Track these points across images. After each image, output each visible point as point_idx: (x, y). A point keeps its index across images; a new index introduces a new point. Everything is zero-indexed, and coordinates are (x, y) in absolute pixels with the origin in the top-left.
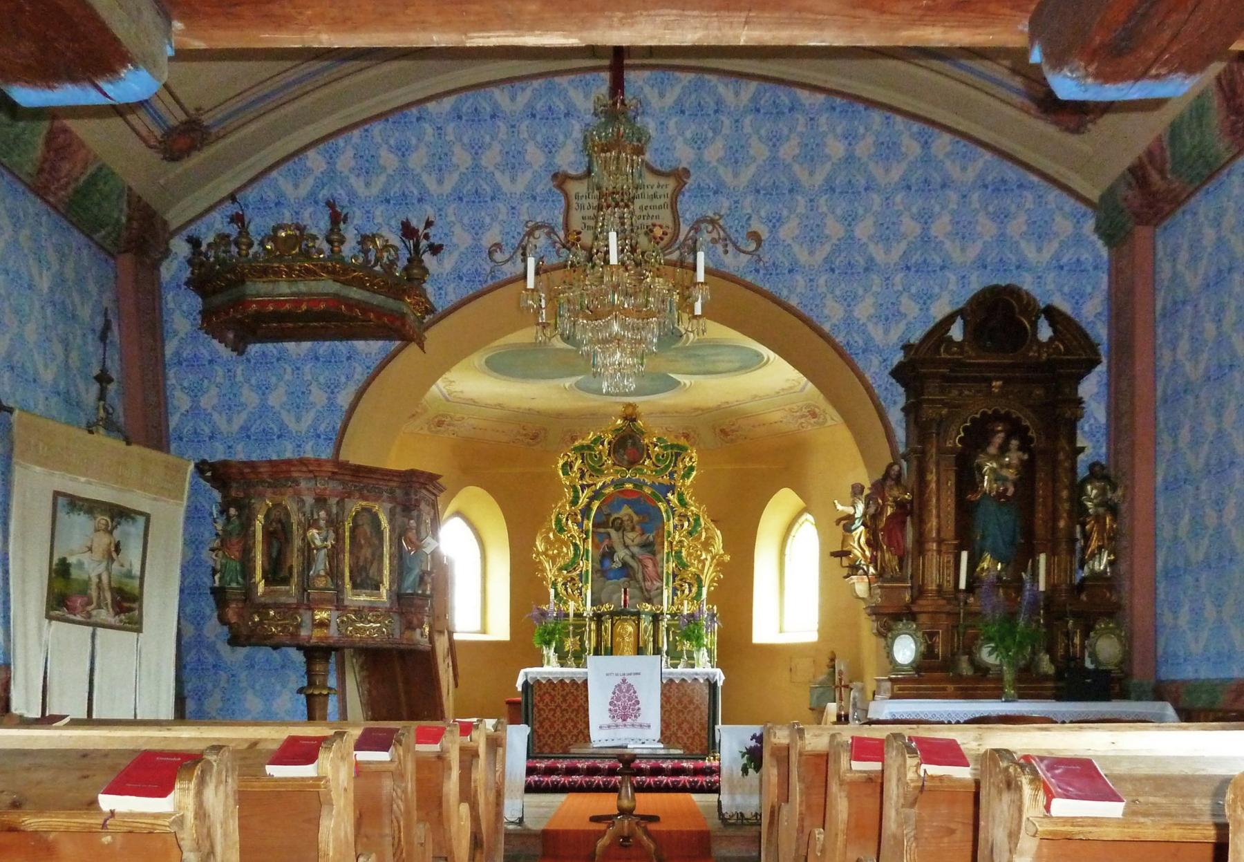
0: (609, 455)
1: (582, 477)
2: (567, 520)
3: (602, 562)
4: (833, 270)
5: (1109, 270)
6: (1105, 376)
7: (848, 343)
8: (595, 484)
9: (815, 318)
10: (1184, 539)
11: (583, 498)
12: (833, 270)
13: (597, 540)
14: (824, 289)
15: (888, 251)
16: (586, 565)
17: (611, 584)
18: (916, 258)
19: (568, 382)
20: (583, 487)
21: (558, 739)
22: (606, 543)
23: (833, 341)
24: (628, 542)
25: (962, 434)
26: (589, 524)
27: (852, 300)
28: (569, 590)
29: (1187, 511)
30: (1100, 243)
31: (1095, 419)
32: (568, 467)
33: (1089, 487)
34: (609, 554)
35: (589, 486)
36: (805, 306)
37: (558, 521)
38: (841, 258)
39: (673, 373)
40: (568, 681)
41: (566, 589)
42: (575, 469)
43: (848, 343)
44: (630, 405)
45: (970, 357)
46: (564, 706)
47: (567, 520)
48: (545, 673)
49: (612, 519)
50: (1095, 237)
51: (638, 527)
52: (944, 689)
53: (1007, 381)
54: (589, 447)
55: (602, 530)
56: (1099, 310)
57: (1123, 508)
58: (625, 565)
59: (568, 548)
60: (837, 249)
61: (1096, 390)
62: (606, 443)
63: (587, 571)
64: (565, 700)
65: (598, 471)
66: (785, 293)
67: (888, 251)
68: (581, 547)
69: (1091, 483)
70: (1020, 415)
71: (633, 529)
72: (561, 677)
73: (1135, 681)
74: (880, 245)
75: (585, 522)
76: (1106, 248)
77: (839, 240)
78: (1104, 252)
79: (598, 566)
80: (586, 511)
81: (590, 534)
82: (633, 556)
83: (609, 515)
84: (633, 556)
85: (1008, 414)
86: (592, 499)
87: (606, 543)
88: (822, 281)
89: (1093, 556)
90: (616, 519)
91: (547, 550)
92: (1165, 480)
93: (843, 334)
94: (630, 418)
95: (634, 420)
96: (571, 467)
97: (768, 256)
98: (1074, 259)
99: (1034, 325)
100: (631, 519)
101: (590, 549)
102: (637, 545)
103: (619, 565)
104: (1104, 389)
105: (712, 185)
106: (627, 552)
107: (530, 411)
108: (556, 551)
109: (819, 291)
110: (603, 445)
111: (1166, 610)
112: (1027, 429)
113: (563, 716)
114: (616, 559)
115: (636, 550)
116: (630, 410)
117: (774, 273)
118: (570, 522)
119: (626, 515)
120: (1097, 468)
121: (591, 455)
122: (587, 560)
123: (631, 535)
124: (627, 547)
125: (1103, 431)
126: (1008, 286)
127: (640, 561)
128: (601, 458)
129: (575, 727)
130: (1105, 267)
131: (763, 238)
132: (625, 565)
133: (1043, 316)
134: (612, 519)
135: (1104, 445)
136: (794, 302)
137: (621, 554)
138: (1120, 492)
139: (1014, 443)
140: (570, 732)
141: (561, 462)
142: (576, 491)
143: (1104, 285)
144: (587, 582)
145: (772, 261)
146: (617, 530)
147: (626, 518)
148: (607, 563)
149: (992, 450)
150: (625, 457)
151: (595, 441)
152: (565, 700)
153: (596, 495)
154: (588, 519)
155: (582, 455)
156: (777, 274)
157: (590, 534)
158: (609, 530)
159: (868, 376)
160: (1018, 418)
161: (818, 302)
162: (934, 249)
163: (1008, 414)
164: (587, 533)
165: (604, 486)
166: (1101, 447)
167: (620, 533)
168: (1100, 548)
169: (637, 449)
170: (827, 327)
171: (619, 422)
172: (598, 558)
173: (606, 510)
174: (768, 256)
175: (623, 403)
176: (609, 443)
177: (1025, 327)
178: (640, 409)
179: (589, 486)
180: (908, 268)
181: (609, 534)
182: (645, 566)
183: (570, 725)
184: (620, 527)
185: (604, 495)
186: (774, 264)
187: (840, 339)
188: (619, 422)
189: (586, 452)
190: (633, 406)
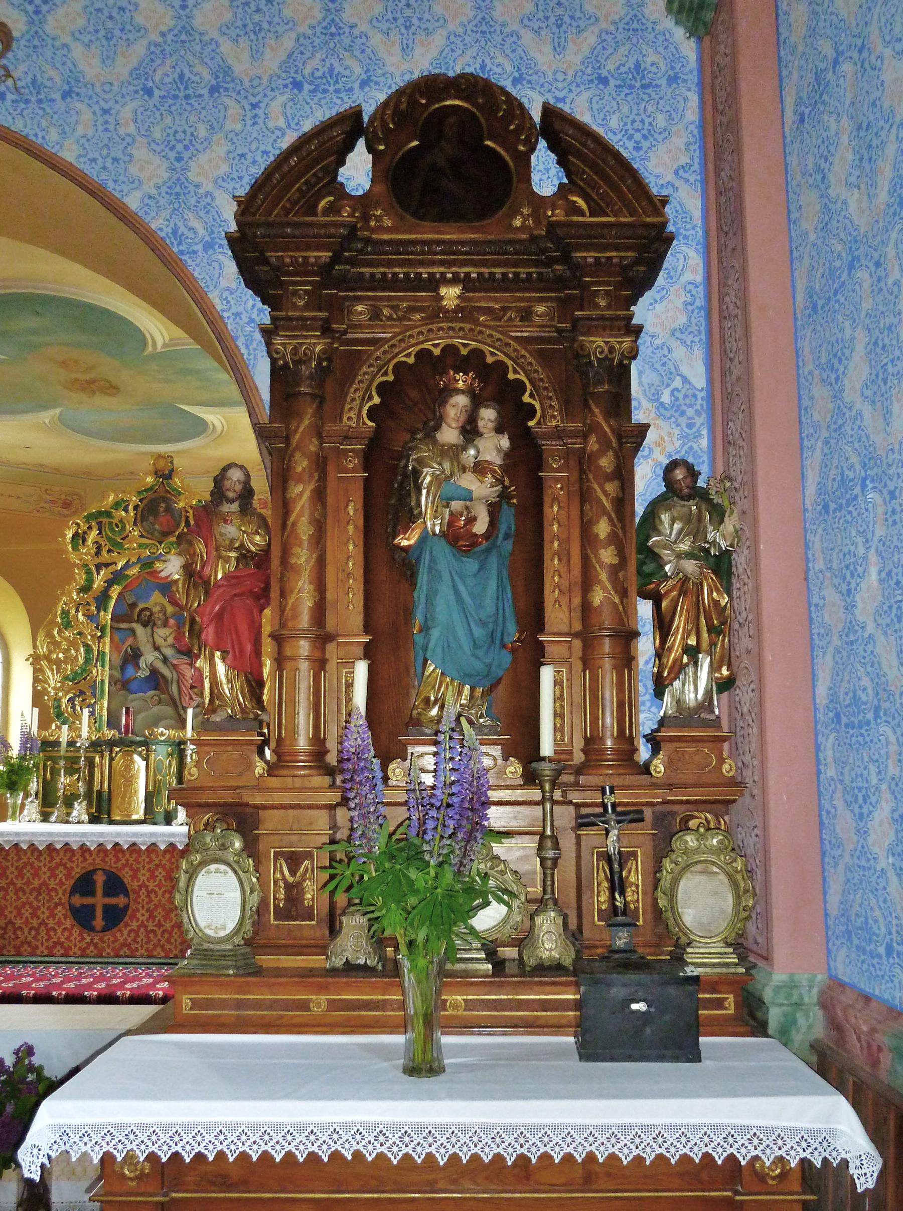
0: (135, 524)
1: (98, 553)
2: (77, 611)
3: (123, 668)
4: (149, 92)
5: (701, 84)
6: (700, 292)
7: (175, 232)
8: (115, 563)
9: (110, 185)
10: (871, 628)
11: (99, 581)
12: (149, 92)
13: (117, 638)
14: (132, 129)
15: (256, 55)
16: (102, 674)
17: (135, 700)
18: (314, 65)
19: (47, 416)
20: (98, 567)
21: (43, 933)
22: (130, 641)
23: (145, 226)
24: (159, 641)
25: (377, 400)
26: (106, 617)
27: (186, 148)
28: (78, 708)
29: (873, 557)
30: (679, 33)
31: (685, 380)
32: (79, 538)
33: (665, 517)
34: (134, 656)
35: (107, 565)
36: (94, 160)
37: (65, 613)
38: (167, 68)
39: (183, 404)
40: (24, 847)
41: (73, 707)
42: (90, 542)
43: (175, 232)
44: (159, 456)
45: (381, 229)
46: (19, 883)
47: (77, 611)
48: (9, 834)
49: (138, 609)
50: (668, 23)
51: (172, 621)
52: (304, 1006)
53: (467, 284)
54: (108, 514)
55: (124, 626)
56: (684, 160)
57: (740, 560)
58: (154, 672)
59: (77, 651)
60: (156, 53)
61: (682, 319)
62: (131, 508)
63: (102, 681)
64: (21, 875)
65: (116, 546)
66: (53, 136)
67: (256, 55)
68: (95, 648)
69: (668, 509)
70: (502, 357)
71: (165, 624)
72: (15, 839)
73: (779, 977)
74: (244, 42)
75: (102, 614)
76: (692, 43)
77: (163, 35)
78: (689, 49)
79: (117, 674)
80: (102, 599)
81: (108, 630)
82: (165, 660)
83: (133, 605)
84: (165, 660)
85: (477, 354)
86: (110, 583)
87: (130, 641)
88: (126, 113)
89: (678, 669)
90: (143, 610)
91: (50, 652)
92: (821, 489)
93: (166, 214)
94: (165, 474)
95: (169, 476)
96: (84, 540)
97: (23, 68)
98: (631, 64)
99: (524, 161)
100: (163, 610)
101: (107, 650)
102: (172, 646)
103: (143, 673)
104: (700, 319)
105: (509, 69)
106: (156, 654)
107: (57, 471)
108: (61, 655)
109: (122, 131)
110: (126, 511)
111: (839, 803)
112: (520, 387)
113: (18, 899)
114: (142, 664)
115: (169, 652)
116: (161, 464)
117: (34, 99)
118: (80, 614)
119: (156, 604)
120: (679, 474)
121: (111, 523)
122: (103, 666)
123: (161, 632)
124: (157, 648)
125: (700, 402)
126: (462, 76)
127: (175, 667)
128: (124, 528)
129: (34, 914)
130: (694, 78)
131: (15, 34)
132: (154, 672)
133: (542, 144)
134: (138, 609)
135: (705, 432)
136: (69, 154)
137: (149, 657)
138: (729, 525)
139: (488, 415)
140: (27, 922)
141: (69, 534)
142: (89, 573)
143: (692, 114)
144: (102, 697)
145: (30, 76)
146: (145, 625)
147: (156, 609)
148: (130, 671)
149: (449, 435)
150: (157, 527)
151: (117, 505)
152: (21, 875)
153: (116, 578)
154: (105, 610)
155: (100, 524)
156: (40, 101)
157: (108, 630)
158: (134, 625)
159: (214, 296)
160: (501, 365)
161: (117, 152)
162: (349, 49)
163: (477, 354)
164: (103, 631)
165: (127, 566)
166: (698, 436)
167: (149, 629)
168: (693, 652)
169: (172, 516)
170: (133, 202)
171: (150, 480)
172: (118, 661)
173: (130, 599)
174: (23, 68)
175: (152, 455)
176: (136, 508)
177: (506, 164)
178: (179, 463)
179: (107, 565)
180: (298, 85)
181: (133, 631)
182: (181, 675)
183: (27, 912)
184: (148, 622)
185: (127, 576)
186: (34, 81)
187: (158, 223)
188: (150, 480)
189: (105, 520)
190: (169, 458)
